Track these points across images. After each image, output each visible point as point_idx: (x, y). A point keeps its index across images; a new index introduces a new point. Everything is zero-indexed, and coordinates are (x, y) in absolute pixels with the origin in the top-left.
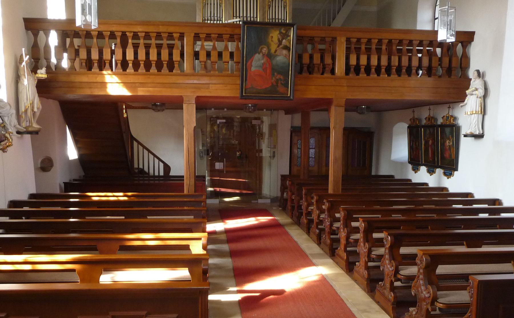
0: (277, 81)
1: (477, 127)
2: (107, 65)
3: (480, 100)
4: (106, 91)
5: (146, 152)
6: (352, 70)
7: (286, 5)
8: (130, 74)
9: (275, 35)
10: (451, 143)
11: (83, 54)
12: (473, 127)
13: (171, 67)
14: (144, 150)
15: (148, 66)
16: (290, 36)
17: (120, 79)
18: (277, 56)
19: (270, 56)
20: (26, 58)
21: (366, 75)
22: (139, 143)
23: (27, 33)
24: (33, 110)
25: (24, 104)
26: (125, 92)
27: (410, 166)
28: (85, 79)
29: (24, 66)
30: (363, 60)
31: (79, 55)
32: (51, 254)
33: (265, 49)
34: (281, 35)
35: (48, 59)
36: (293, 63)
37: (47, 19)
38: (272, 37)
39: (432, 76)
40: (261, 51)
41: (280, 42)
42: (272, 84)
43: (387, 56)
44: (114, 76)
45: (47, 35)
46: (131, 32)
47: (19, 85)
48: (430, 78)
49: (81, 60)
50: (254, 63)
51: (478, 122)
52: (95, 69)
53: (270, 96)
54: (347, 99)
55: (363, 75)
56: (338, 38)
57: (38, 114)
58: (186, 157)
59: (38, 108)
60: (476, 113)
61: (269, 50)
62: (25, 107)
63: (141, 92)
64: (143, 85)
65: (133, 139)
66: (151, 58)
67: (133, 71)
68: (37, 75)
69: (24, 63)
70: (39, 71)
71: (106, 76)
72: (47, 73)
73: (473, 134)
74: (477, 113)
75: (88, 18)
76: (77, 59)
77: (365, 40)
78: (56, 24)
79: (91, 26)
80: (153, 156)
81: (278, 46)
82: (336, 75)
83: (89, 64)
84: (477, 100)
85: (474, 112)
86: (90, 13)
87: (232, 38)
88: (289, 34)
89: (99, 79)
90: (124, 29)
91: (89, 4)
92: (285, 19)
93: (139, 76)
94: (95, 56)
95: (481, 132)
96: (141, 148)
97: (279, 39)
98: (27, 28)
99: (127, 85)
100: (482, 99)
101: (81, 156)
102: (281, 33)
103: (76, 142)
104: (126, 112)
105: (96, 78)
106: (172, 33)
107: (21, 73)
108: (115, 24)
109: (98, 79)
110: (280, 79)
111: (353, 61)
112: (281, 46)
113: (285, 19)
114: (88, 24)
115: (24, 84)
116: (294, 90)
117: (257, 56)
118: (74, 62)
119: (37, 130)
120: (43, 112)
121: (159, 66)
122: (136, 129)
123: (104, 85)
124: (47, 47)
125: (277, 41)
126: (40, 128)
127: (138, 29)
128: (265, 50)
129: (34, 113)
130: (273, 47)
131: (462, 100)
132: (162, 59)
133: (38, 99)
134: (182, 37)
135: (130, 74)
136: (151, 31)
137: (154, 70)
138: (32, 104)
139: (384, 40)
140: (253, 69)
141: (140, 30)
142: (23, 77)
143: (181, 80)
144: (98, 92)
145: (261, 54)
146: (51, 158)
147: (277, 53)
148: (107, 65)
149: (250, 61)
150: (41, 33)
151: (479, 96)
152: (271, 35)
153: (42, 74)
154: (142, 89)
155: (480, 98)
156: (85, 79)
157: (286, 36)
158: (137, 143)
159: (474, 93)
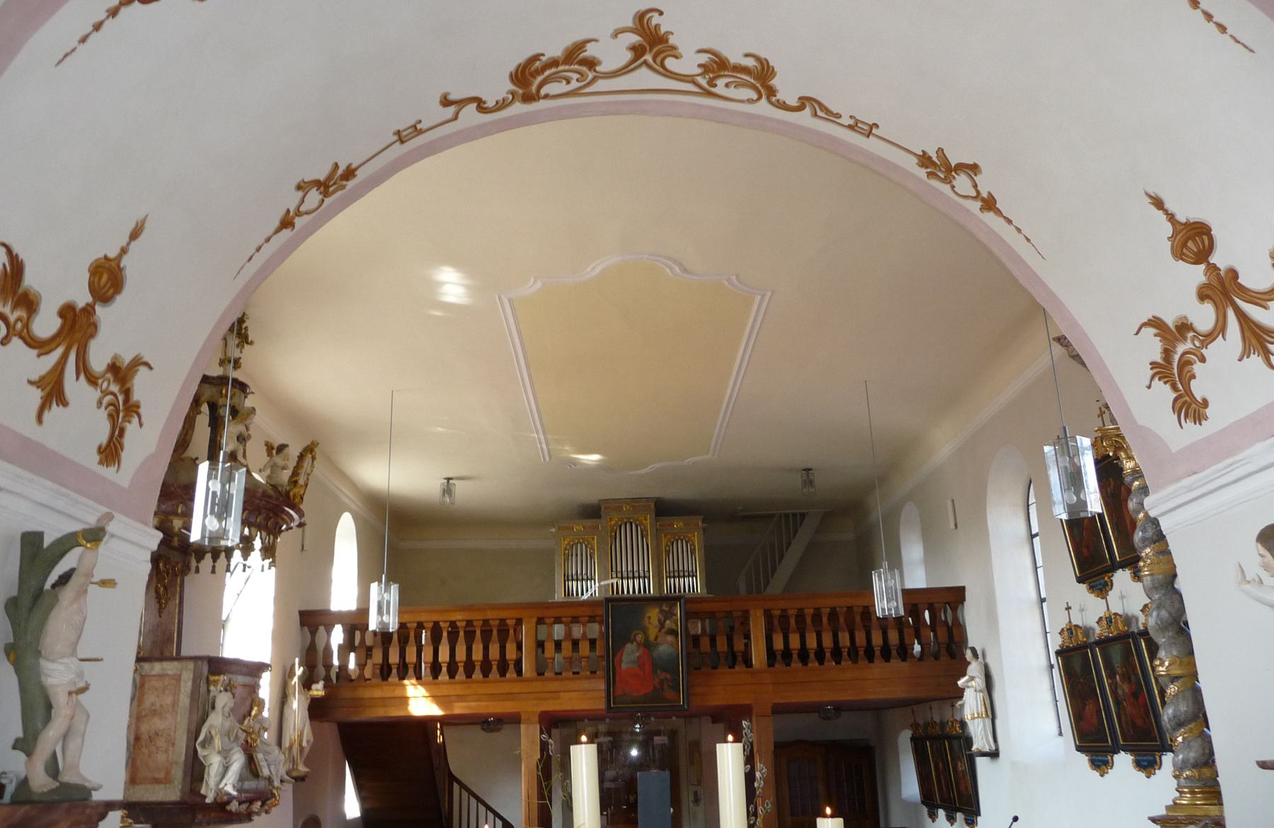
0: (661, 682)
1: (984, 740)
2: (411, 671)
3: (981, 694)
4: (407, 709)
5: (473, 801)
6: (779, 657)
7: (695, 549)
8: (444, 683)
9: (653, 615)
10: (964, 767)
11: (378, 657)
12: (980, 738)
13: (503, 670)
14: (471, 797)
15: (469, 668)
16: (676, 615)
17: (427, 690)
18: (658, 644)
19: (648, 646)
20: (299, 671)
21: (801, 665)
22: (462, 786)
23: (302, 629)
24: (300, 745)
25: (290, 734)
26: (433, 710)
27: (925, 810)
28: (377, 693)
29: (295, 683)
30: (795, 642)
31: (371, 655)
32: (343, 745)
33: (640, 636)
34: (663, 614)
35: (328, 666)
36: (684, 653)
37: (330, 610)
38: (650, 618)
39: (908, 659)
40: (635, 639)
41: (662, 625)
42: (654, 686)
43: (831, 633)
44: (419, 687)
45: (329, 632)
46: (446, 622)
47: (286, 707)
48: (904, 664)
49: (374, 665)
50: (624, 658)
51: (985, 731)
52: (393, 678)
53: (650, 707)
54: (774, 704)
55: (796, 664)
56: (752, 612)
57: (307, 751)
58: (525, 810)
59: (308, 742)
60: (978, 717)
61: (647, 637)
62: (291, 740)
63: (459, 709)
64: (461, 698)
65: (452, 778)
66: (474, 658)
67: (448, 677)
68: (311, 693)
69: (296, 679)
70: (314, 686)
71: (407, 687)
72: (325, 687)
73: (981, 751)
74: (980, 715)
75: (385, 618)
76: (369, 662)
77: (793, 611)
78: (341, 617)
79: (389, 629)
80: (484, 809)
81: (660, 631)
82: (754, 667)
83: (385, 671)
84: (976, 695)
85: (976, 715)
86: (388, 612)
87: (592, 619)
88: (675, 612)
89: (397, 693)
90: (436, 618)
91: (387, 601)
92: (694, 570)
93: (457, 686)
94: (394, 658)
95: (994, 748)
96: (465, 794)
97: (659, 620)
98: (303, 624)
99: (437, 698)
100: (986, 692)
101: (364, 811)
102: (662, 611)
103: (359, 787)
104: (442, 733)
105: (394, 690)
106: (505, 620)
107: (290, 691)
108: (424, 611)
109: (396, 692)
110: (667, 679)
111: (779, 644)
112: (663, 631)
113: (694, 570)
114: (386, 625)
115: (292, 708)
116: (688, 696)
117: (629, 647)
118: (364, 669)
119: (303, 774)
120: (314, 749)
121: (486, 669)
122: (456, 764)
123: (404, 700)
124: (328, 649)
125: (657, 623)
126: (308, 772)
127: (458, 617)
128: (640, 637)
129: (302, 749)
130: (653, 632)
131: (957, 695)
132: (491, 658)
133: (309, 727)
134: (519, 622)
135: (444, 683)
136: (474, 618)
137: (477, 675)
138: (301, 736)
139: (823, 609)
140: (624, 666)
141: (459, 617)
142: (292, 697)
143: (516, 688)
144: (395, 712)
145: (635, 644)
146: (317, 817)
147: (658, 641)
148: (411, 671)
149: (619, 654)
150: (322, 629)
151: (978, 688)
152: (648, 615)
153: (318, 690)
154: (460, 704)
155: (981, 691)
156: (377, 693)
157: (669, 615)
158: (458, 786)
159: (969, 684)
